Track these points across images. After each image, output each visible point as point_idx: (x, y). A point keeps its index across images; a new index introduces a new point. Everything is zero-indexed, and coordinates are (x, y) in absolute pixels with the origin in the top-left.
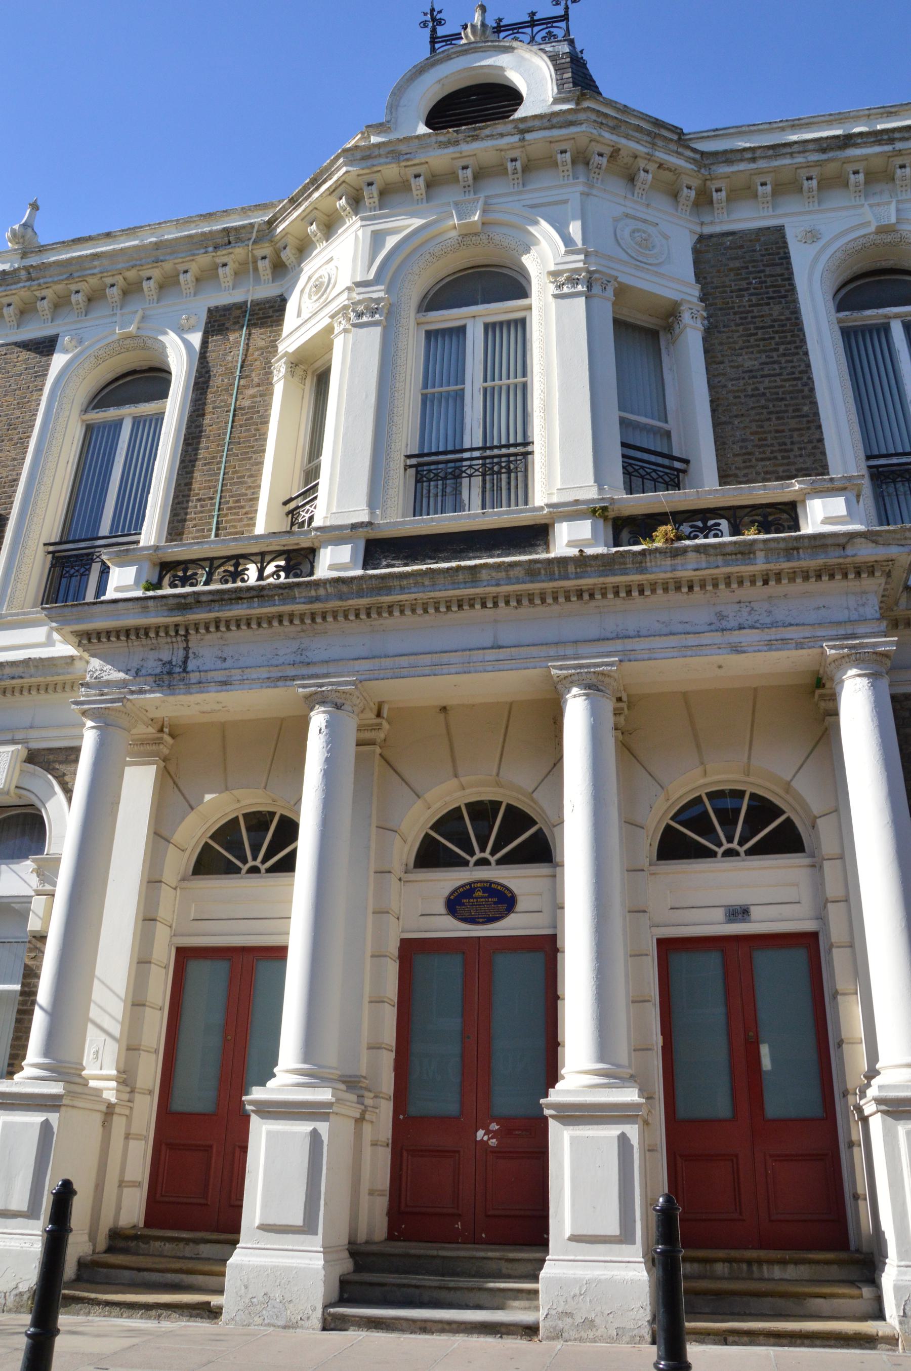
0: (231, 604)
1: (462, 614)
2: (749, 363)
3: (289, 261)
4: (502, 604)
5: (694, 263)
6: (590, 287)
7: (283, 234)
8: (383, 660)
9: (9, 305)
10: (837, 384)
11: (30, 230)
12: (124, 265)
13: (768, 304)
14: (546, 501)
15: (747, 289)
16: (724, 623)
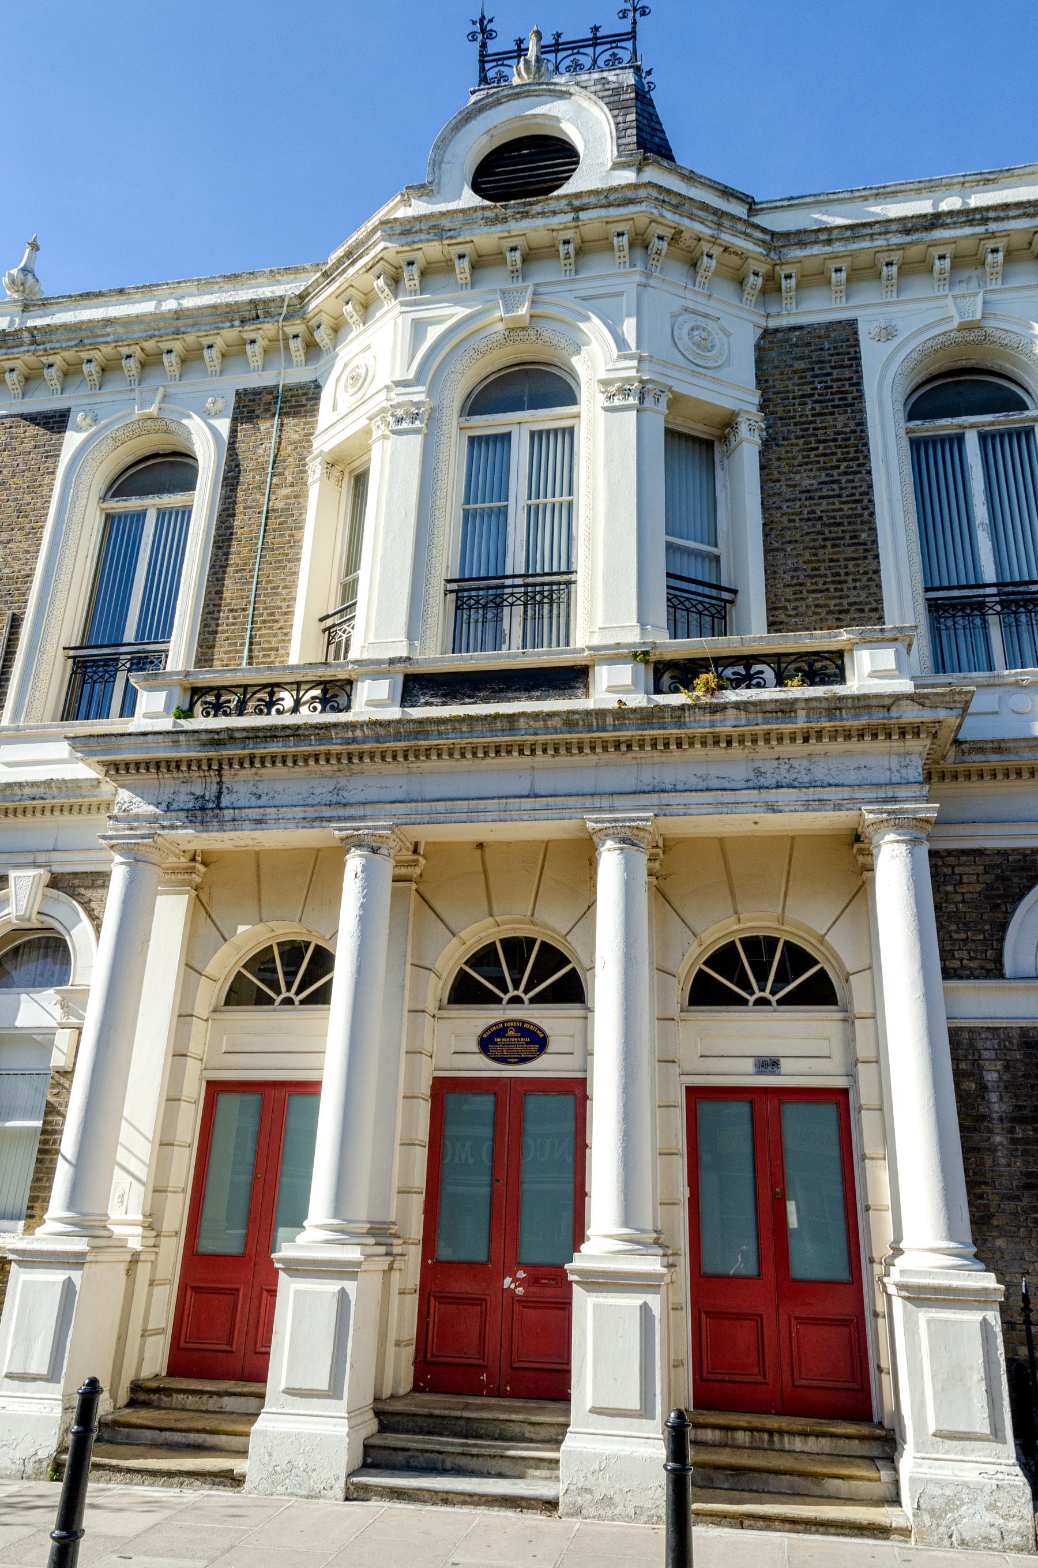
0: (266, 741)
1: (498, 760)
2: (806, 480)
3: (324, 343)
4: (539, 752)
5: (756, 362)
6: (642, 400)
7: (317, 310)
8: (420, 804)
9: (12, 370)
10: (898, 506)
11: (30, 276)
12: (140, 335)
13: (833, 414)
14: (587, 644)
15: (811, 395)
16: (762, 780)
